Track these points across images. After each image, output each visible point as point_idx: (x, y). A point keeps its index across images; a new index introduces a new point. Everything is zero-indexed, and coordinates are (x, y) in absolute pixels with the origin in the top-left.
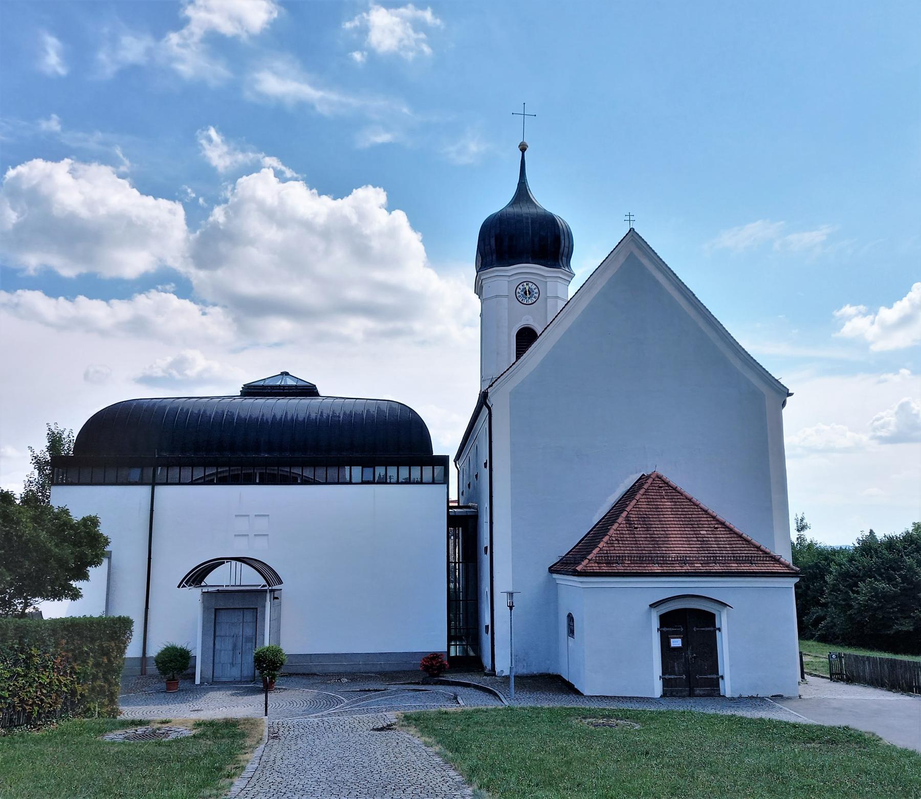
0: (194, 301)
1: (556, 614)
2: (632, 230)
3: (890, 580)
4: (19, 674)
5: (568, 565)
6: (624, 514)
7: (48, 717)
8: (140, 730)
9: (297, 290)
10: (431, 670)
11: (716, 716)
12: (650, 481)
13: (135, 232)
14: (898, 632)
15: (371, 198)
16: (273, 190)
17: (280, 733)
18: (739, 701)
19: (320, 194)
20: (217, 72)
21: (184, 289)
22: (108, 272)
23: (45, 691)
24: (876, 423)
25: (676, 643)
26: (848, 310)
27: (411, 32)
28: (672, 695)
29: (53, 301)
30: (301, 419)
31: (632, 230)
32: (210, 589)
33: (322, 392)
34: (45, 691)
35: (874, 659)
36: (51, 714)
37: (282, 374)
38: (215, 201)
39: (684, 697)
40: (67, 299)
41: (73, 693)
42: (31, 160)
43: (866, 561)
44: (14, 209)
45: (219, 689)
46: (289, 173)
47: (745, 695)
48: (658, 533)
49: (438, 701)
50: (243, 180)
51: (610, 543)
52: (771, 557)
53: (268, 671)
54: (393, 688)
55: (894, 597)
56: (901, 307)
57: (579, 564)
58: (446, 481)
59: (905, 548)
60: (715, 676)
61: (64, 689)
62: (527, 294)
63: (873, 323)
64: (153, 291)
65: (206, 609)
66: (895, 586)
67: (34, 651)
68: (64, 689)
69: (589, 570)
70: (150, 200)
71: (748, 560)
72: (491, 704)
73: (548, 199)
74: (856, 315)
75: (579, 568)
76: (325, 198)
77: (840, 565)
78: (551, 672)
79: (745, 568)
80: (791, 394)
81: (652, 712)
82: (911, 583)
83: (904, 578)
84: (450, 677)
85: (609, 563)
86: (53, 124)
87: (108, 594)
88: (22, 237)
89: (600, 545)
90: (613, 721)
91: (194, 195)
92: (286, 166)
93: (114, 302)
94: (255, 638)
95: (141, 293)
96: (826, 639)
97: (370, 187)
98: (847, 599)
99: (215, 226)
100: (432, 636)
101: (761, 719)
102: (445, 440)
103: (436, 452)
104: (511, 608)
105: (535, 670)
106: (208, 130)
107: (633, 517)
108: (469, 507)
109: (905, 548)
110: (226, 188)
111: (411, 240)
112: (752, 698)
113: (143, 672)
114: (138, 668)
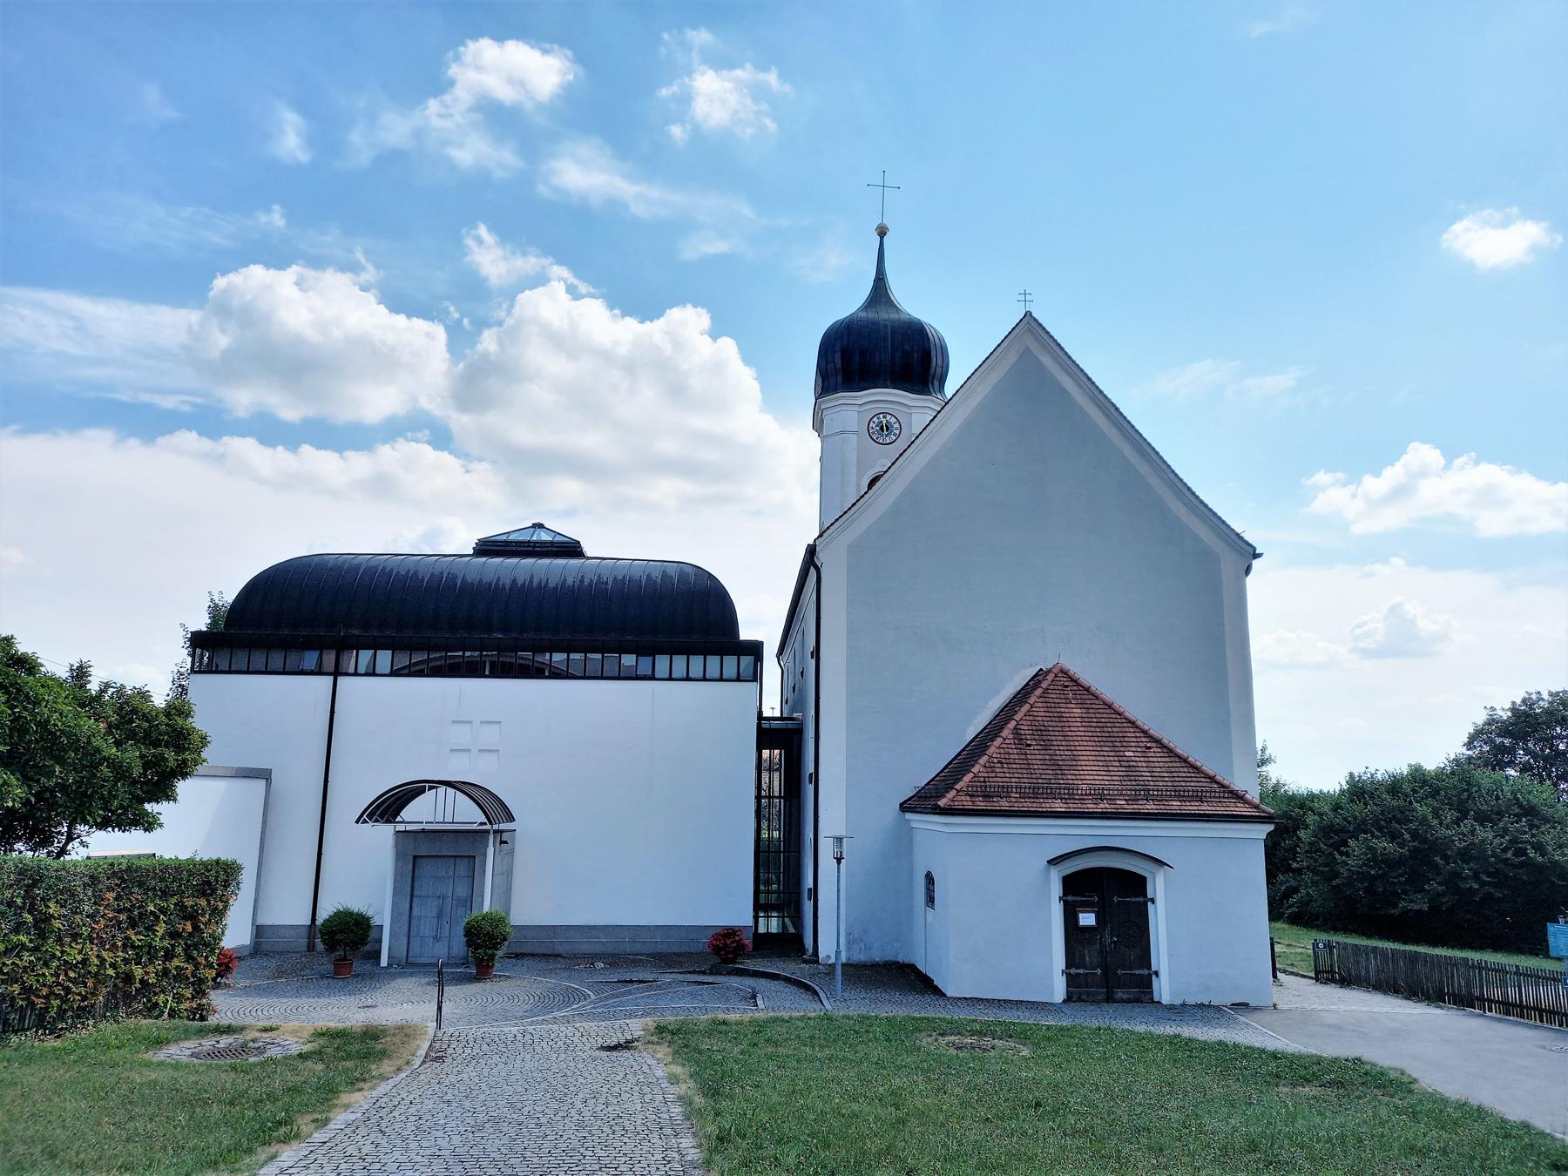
0: (455, 453)
1: (911, 872)
2: (1028, 314)
3: (1394, 837)
4: (23, 945)
5: (925, 801)
6: (1012, 724)
7: (79, 1017)
8: (225, 1041)
9: (592, 441)
10: (725, 953)
11: (1150, 1037)
12: (1050, 677)
13: (380, 361)
14: (1406, 912)
15: (689, 321)
16: (561, 309)
17: (450, 1051)
18: (1181, 1011)
19: (623, 315)
20: (500, 158)
21: (441, 438)
22: (343, 414)
23: (72, 975)
24: (1358, 631)
25: (1087, 919)
26: (1322, 477)
27: (749, 102)
28: (1080, 1000)
29: (268, 452)
30: (552, 585)
31: (1028, 314)
32: (410, 827)
33: (589, 550)
34: (72, 975)
35: (1383, 952)
36: (83, 1013)
37: (534, 526)
38: (482, 324)
39: (1099, 1002)
40: (286, 448)
41: (128, 978)
42: (247, 266)
43: (1357, 808)
44: (223, 331)
45: (411, 975)
46: (583, 288)
47: (1191, 1001)
48: (1062, 753)
49: (727, 1000)
50: (525, 297)
51: (989, 767)
52: (1231, 792)
53: (485, 949)
54: (667, 978)
55: (1401, 861)
56: (1393, 474)
57: (943, 796)
58: (756, 676)
59: (1414, 791)
60: (1146, 972)
61: (111, 972)
62: (883, 430)
63: (1354, 496)
64: (401, 440)
65: (400, 855)
66: (1401, 846)
67: (53, 908)
68: (111, 972)
69: (957, 805)
70: (401, 320)
71: (1201, 797)
72: (810, 1008)
73: (914, 300)
74: (1333, 485)
75: (942, 803)
76: (628, 320)
77: (1321, 815)
78: (900, 959)
79: (1193, 807)
80: (1260, 555)
81: (1049, 1028)
82: (1425, 840)
83: (1415, 835)
84: (751, 965)
85: (986, 797)
86: (276, 218)
87: (263, 833)
88: (234, 366)
89: (975, 770)
90: (988, 1041)
91: (457, 315)
92: (579, 278)
93: (349, 454)
94: (469, 900)
95: (384, 441)
96: (1301, 919)
97: (689, 306)
98: (1331, 863)
99: (485, 357)
100: (731, 904)
101: (1220, 1043)
102: (760, 615)
103: (745, 634)
104: (839, 860)
105: (877, 956)
106: (476, 228)
107: (1025, 729)
108: (792, 719)
109: (1414, 791)
110: (500, 306)
111: (743, 378)
112: (1201, 1006)
113: (311, 947)
114: (304, 942)
